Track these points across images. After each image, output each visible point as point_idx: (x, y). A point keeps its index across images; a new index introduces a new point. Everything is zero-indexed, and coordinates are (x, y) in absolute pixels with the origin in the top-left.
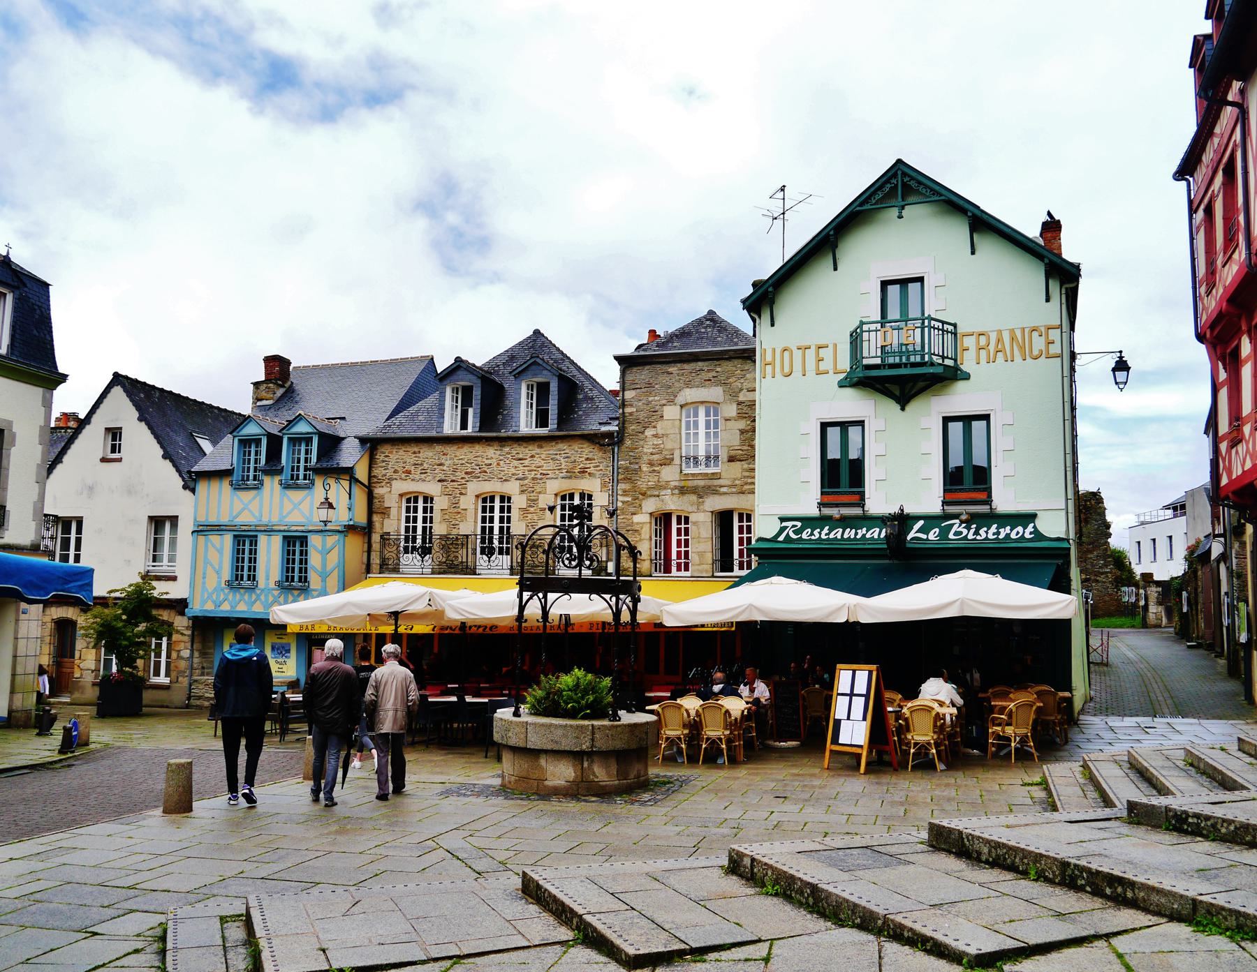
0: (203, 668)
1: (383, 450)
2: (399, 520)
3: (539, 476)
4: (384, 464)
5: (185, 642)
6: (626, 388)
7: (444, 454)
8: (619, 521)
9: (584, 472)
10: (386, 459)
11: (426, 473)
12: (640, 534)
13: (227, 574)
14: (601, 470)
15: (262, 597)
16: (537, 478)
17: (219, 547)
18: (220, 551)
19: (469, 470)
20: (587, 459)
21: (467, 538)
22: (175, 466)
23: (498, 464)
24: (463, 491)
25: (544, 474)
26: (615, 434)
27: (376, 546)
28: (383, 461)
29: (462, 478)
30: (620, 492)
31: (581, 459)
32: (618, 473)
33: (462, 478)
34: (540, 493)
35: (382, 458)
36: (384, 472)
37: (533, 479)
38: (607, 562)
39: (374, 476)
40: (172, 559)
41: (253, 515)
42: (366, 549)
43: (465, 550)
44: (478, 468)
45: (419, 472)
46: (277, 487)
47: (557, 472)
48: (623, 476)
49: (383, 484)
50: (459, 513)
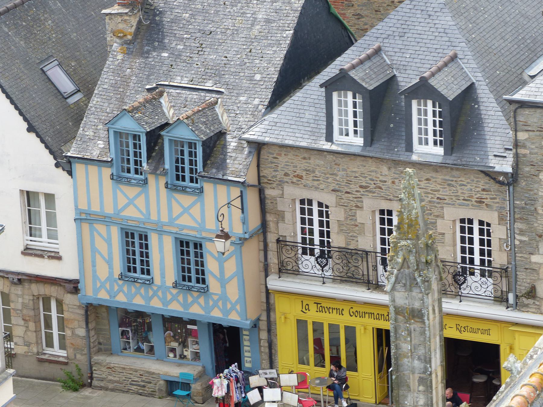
0: (100, 343)
1: (270, 151)
2: (295, 223)
3: (435, 200)
4: (273, 165)
5: (79, 321)
6: (518, 129)
7: (336, 164)
8: (517, 258)
9: (481, 202)
10: (275, 160)
11: (318, 180)
12: (538, 274)
13: (118, 266)
14: (498, 203)
15: (160, 294)
16: (434, 202)
17: (106, 237)
18: (109, 241)
19: (364, 184)
20: (484, 190)
21: (367, 254)
22: (38, 136)
23: (393, 183)
24: (359, 204)
25: (441, 199)
26: (510, 175)
27: (272, 246)
28: (272, 163)
29: (357, 191)
30: (517, 231)
31: (478, 189)
32: (514, 212)
33: (357, 191)
34: (437, 216)
35: (270, 159)
36: (274, 173)
37: (430, 202)
38: (508, 292)
39: (264, 176)
40: (52, 235)
41: (141, 212)
42: (262, 247)
43: (365, 263)
44: (372, 182)
45: (311, 178)
46: (163, 191)
47: (454, 198)
48: (519, 216)
49: (274, 185)
50: (357, 226)
